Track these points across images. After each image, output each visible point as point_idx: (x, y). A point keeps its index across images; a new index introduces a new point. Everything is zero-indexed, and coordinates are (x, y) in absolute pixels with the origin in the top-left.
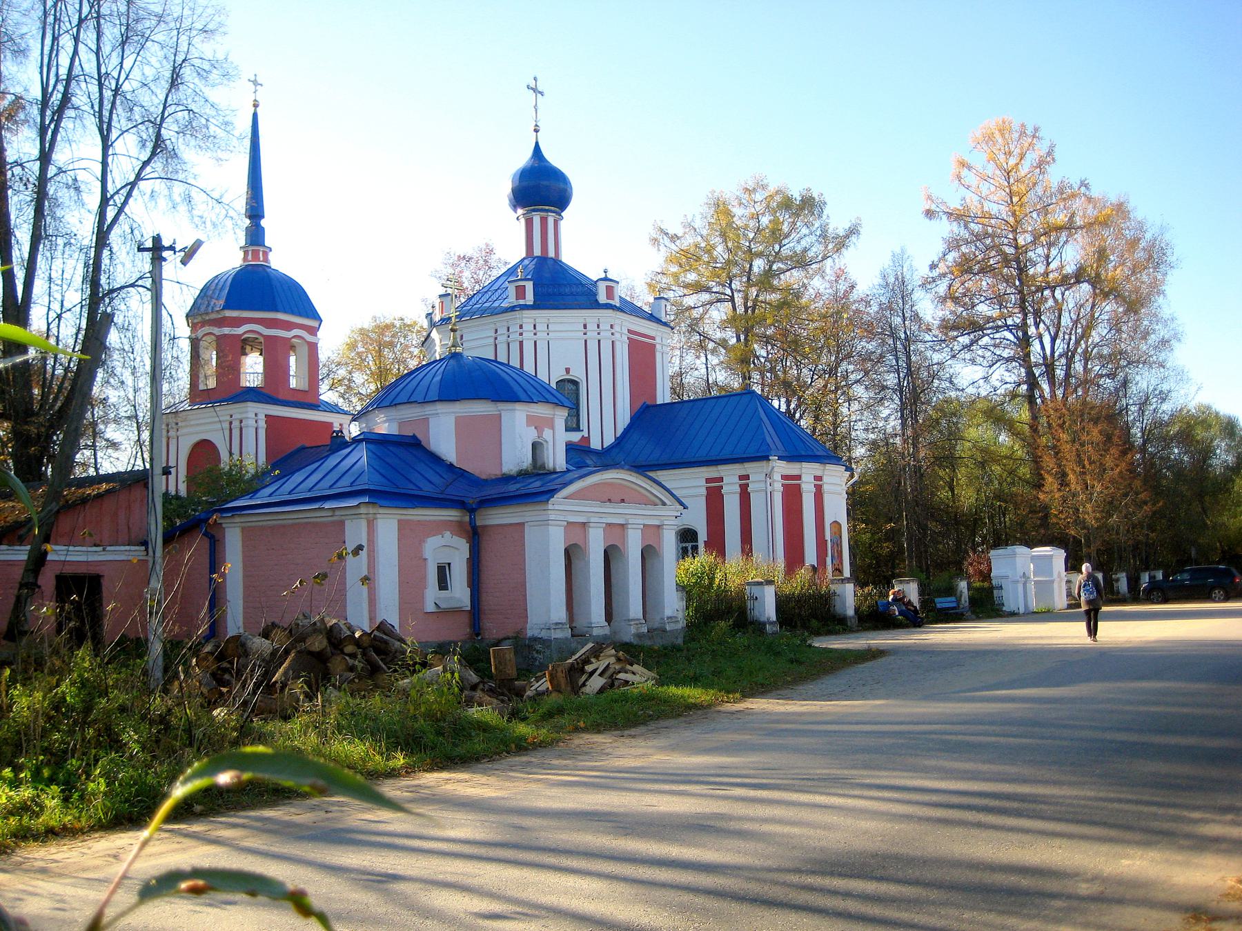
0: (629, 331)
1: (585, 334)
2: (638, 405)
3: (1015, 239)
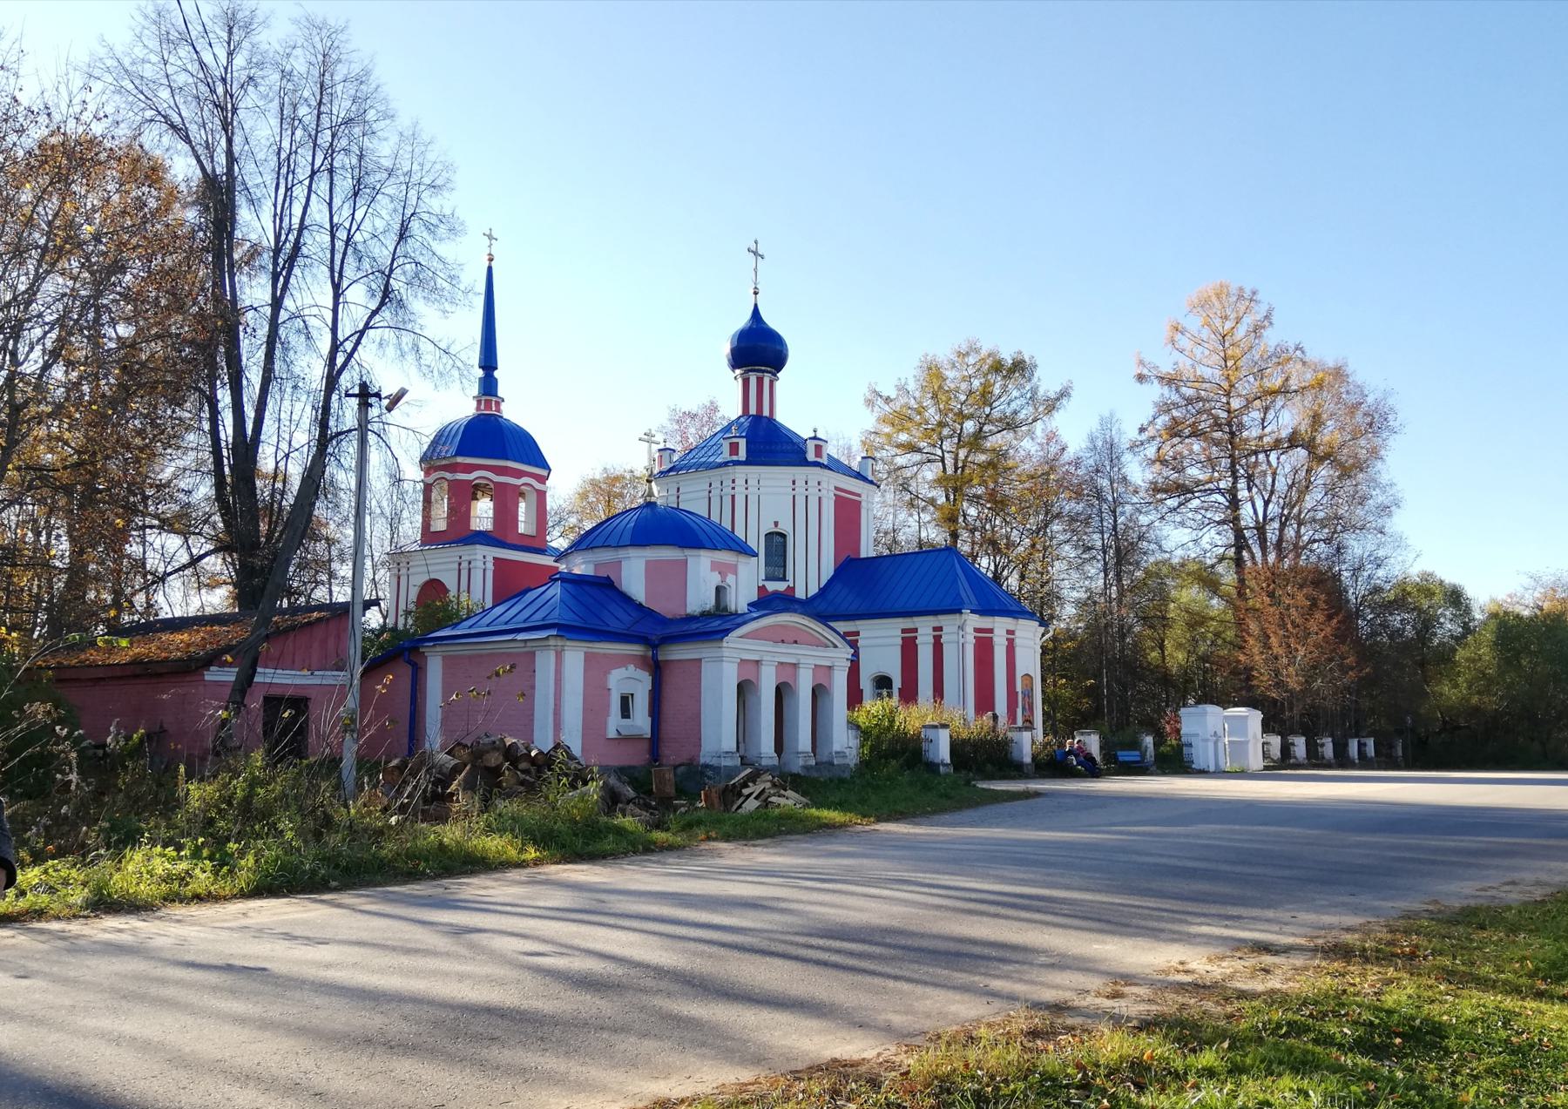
0: (836, 488)
1: (794, 490)
2: (842, 558)
3: (1228, 403)
